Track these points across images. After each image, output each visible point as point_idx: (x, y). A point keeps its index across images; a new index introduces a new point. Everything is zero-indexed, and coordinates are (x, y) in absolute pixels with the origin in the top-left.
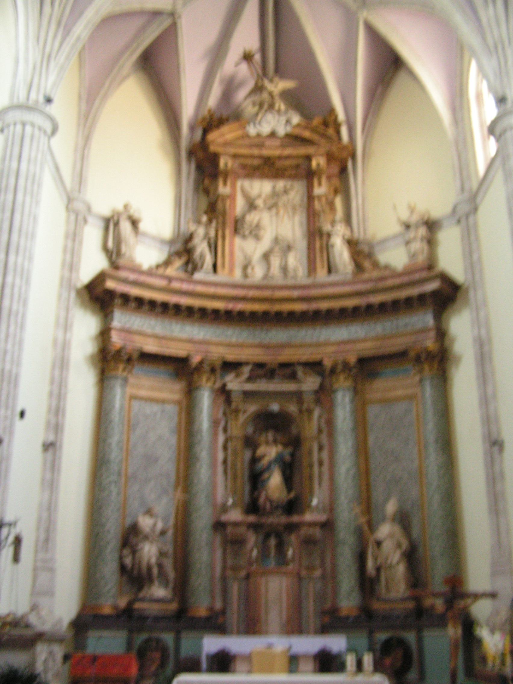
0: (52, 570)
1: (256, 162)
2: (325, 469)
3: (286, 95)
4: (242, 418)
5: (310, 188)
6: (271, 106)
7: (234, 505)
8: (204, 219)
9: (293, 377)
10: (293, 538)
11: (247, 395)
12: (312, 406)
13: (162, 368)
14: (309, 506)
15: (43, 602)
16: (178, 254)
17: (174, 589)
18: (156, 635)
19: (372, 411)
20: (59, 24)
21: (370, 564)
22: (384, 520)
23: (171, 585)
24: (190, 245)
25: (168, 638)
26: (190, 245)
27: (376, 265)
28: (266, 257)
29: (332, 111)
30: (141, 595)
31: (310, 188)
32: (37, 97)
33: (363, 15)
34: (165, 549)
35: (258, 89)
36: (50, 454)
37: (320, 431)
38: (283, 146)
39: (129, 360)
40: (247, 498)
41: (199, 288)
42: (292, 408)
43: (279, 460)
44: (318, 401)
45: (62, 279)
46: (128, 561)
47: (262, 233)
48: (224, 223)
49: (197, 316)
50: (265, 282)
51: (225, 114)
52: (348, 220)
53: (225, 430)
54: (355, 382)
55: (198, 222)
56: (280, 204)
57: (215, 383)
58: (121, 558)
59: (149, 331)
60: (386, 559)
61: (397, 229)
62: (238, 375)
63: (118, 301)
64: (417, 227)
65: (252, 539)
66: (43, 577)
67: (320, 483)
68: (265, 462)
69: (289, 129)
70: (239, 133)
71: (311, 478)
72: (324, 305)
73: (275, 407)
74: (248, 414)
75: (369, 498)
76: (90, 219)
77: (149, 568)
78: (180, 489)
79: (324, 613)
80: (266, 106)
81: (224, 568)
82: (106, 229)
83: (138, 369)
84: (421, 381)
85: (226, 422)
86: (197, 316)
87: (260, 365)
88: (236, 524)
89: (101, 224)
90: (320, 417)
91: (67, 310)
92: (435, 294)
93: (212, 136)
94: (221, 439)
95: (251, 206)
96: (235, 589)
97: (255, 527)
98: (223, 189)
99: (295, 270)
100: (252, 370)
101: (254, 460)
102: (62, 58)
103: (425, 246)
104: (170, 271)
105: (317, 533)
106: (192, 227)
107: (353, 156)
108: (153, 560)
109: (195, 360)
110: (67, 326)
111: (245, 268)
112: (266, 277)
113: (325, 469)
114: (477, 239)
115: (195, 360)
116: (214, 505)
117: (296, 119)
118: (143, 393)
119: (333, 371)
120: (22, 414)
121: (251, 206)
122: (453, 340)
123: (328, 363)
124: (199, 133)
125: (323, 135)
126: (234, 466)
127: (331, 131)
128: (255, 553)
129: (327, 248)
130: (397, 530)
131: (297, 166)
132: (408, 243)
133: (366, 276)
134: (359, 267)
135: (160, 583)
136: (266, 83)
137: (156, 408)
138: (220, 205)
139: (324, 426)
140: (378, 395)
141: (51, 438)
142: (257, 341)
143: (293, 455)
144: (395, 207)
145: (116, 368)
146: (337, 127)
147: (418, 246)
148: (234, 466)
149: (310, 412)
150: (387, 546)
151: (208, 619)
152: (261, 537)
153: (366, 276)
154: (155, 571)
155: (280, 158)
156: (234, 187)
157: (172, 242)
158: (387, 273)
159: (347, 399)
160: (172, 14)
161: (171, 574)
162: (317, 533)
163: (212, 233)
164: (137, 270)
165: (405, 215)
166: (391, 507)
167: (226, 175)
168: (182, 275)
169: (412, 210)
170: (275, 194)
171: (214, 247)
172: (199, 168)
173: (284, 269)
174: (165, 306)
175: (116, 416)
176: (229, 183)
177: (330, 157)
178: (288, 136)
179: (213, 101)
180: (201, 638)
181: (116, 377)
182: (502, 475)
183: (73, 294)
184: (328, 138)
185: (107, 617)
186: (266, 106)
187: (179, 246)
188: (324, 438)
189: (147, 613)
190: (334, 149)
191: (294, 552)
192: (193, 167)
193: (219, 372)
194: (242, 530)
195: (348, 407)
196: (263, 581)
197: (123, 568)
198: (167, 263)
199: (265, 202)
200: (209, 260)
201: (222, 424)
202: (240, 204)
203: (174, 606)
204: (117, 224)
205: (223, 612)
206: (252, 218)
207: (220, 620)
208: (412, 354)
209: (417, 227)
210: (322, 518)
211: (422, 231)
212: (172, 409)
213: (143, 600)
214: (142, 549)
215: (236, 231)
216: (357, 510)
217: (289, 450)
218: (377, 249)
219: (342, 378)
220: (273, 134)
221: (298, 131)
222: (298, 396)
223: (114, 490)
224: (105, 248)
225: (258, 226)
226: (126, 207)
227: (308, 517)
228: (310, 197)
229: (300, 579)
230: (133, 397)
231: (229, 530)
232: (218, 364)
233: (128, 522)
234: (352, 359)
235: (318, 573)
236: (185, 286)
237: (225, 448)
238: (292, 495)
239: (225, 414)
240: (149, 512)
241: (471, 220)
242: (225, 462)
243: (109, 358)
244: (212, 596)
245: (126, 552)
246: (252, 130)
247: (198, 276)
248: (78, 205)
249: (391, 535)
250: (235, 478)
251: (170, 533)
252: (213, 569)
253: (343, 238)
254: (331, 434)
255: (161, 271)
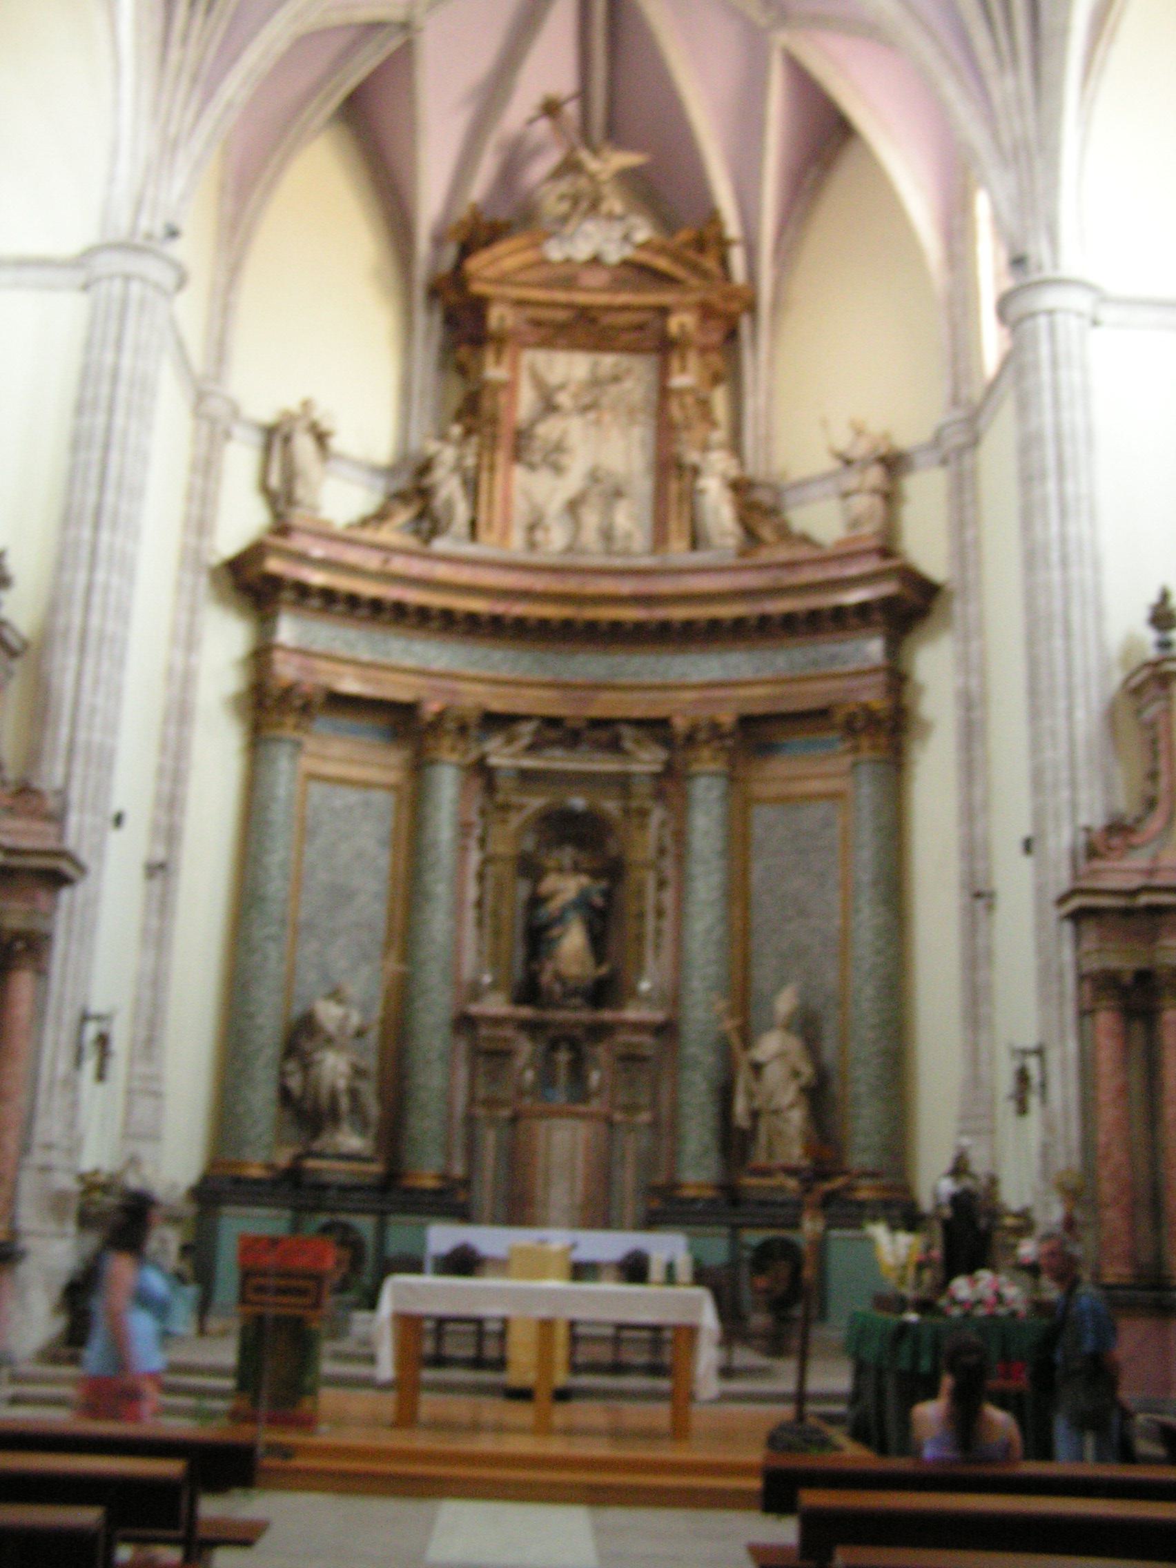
0: (157, 1095)
1: (561, 315)
2: (667, 924)
3: (627, 177)
4: (515, 820)
5: (664, 373)
6: (594, 206)
7: (494, 986)
8: (456, 430)
9: (614, 746)
10: (601, 1051)
11: (526, 777)
12: (648, 804)
13: (366, 722)
14: (634, 993)
15: (144, 1150)
16: (400, 497)
17: (379, 1138)
18: (343, 1217)
19: (763, 816)
20: (194, 79)
21: (740, 1106)
22: (770, 1027)
23: (373, 1130)
24: (427, 481)
25: (364, 1224)
26: (427, 481)
27: (785, 534)
28: (573, 507)
29: (713, 218)
30: (317, 1145)
31: (664, 373)
32: (151, 223)
33: (782, 38)
34: (363, 1064)
35: (570, 167)
36: (157, 884)
37: (662, 851)
38: (617, 285)
39: (306, 709)
40: (518, 973)
41: (442, 571)
42: (611, 806)
43: (583, 903)
44: (659, 795)
45: (184, 550)
46: (295, 1083)
47: (565, 460)
48: (494, 438)
49: (435, 624)
50: (568, 560)
51: (503, 214)
52: (735, 446)
53: (482, 842)
54: (732, 764)
55: (443, 437)
56: (605, 401)
57: (466, 752)
58: (283, 1074)
59: (343, 652)
60: (771, 1095)
61: (828, 464)
62: (510, 741)
63: (288, 595)
64: (865, 464)
65: (525, 1048)
66: (144, 1107)
67: (657, 947)
68: (554, 906)
69: (628, 252)
70: (530, 256)
71: (639, 938)
72: (679, 613)
73: (578, 802)
74: (528, 812)
75: (746, 979)
76: (239, 431)
77: (334, 1096)
78: (394, 955)
79: (654, 1191)
80: (584, 205)
81: (472, 1100)
82: (267, 449)
83: (323, 724)
84: (855, 765)
85: (485, 829)
86: (435, 624)
87: (552, 722)
88: (497, 1021)
89: (256, 439)
90: (663, 824)
91: (193, 611)
92: (887, 605)
93: (478, 264)
94: (475, 857)
95: (549, 407)
96: (490, 1139)
97: (531, 1028)
98: (495, 372)
99: (628, 536)
100: (537, 733)
101: (536, 901)
102: (197, 145)
103: (877, 503)
104: (387, 534)
105: (646, 1042)
106: (433, 447)
107: (751, 307)
108: (342, 1084)
109: (432, 708)
110: (188, 640)
111: (532, 528)
112: (569, 549)
113: (667, 924)
114: (975, 502)
115: (432, 708)
116: (457, 983)
117: (643, 232)
118: (331, 769)
119: (691, 739)
120: (118, 820)
121: (549, 407)
122: (919, 690)
123: (680, 724)
124: (450, 253)
125: (696, 269)
126: (496, 914)
127: (710, 263)
128: (529, 1075)
129: (691, 497)
130: (794, 1044)
131: (640, 327)
132: (846, 495)
133: (765, 556)
134: (751, 536)
135: (353, 1125)
136: (584, 156)
137: (352, 797)
138: (486, 404)
139: (669, 842)
140: (772, 790)
141: (160, 854)
142: (547, 677)
143: (608, 895)
144: (824, 423)
145: (280, 725)
146: (723, 244)
147: (864, 503)
148: (496, 914)
149: (643, 813)
150: (774, 1074)
151: (437, 1192)
152: (542, 1047)
153: (765, 556)
154: (344, 1103)
155: (609, 309)
156: (514, 367)
157: (390, 472)
158: (801, 552)
159: (715, 793)
160: (406, 26)
161: (374, 1109)
162: (646, 1042)
163: (470, 461)
164: (326, 535)
165: (843, 440)
166: (785, 1003)
167: (500, 341)
168: (411, 542)
169: (859, 432)
170: (596, 382)
171: (472, 487)
172: (450, 320)
173: (607, 534)
174: (376, 606)
175: (278, 813)
176: (506, 359)
177: (706, 312)
178: (626, 263)
179: (478, 189)
180: (423, 1226)
181: (279, 740)
182: (989, 953)
183: (204, 581)
184: (704, 274)
185: (257, 1182)
186: (584, 205)
187: (403, 482)
188: (668, 865)
189: (328, 1178)
190: (715, 298)
191: (602, 1079)
192: (438, 318)
193: (473, 732)
194: (508, 1032)
195: (717, 810)
196: (541, 1126)
197: (285, 1095)
198: (380, 517)
199: (575, 396)
200: (462, 511)
201: (477, 832)
202: (526, 401)
203: (376, 1168)
204: (287, 440)
205: (466, 1183)
206: (548, 430)
207: (461, 1197)
208: (839, 717)
209: (865, 464)
210: (658, 1016)
211: (875, 475)
212: (383, 800)
213: (320, 1155)
214: (320, 1062)
215: (517, 455)
216: (722, 1005)
217: (603, 884)
218: (789, 498)
219: (706, 753)
220: (596, 261)
221: (644, 257)
222: (622, 783)
223: (273, 951)
224: (264, 488)
225: (559, 447)
226: (307, 405)
227: (632, 1013)
228: (664, 392)
229: (610, 1122)
230: (313, 777)
231: (484, 1031)
232: (473, 719)
233: (298, 1009)
234: (727, 718)
235: (645, 1117)
236: (417, 568)
237: (481, 877)
238: (604, 970)
239: (483, 813)
240: (336, 995)
241: (967, 460)
242: (479, 904)
243: (269, 702)
244: (448, 1155)
245: (292, 1066)
246: (555, 251)
247: (441, 545)
248: (215, 406)
249: (781, 1055)
250: (497, 933)
251: (373, 1036)
252: (450, 1103)
253: (724, 476)
254: (681, 858)
255: (368, 534)
